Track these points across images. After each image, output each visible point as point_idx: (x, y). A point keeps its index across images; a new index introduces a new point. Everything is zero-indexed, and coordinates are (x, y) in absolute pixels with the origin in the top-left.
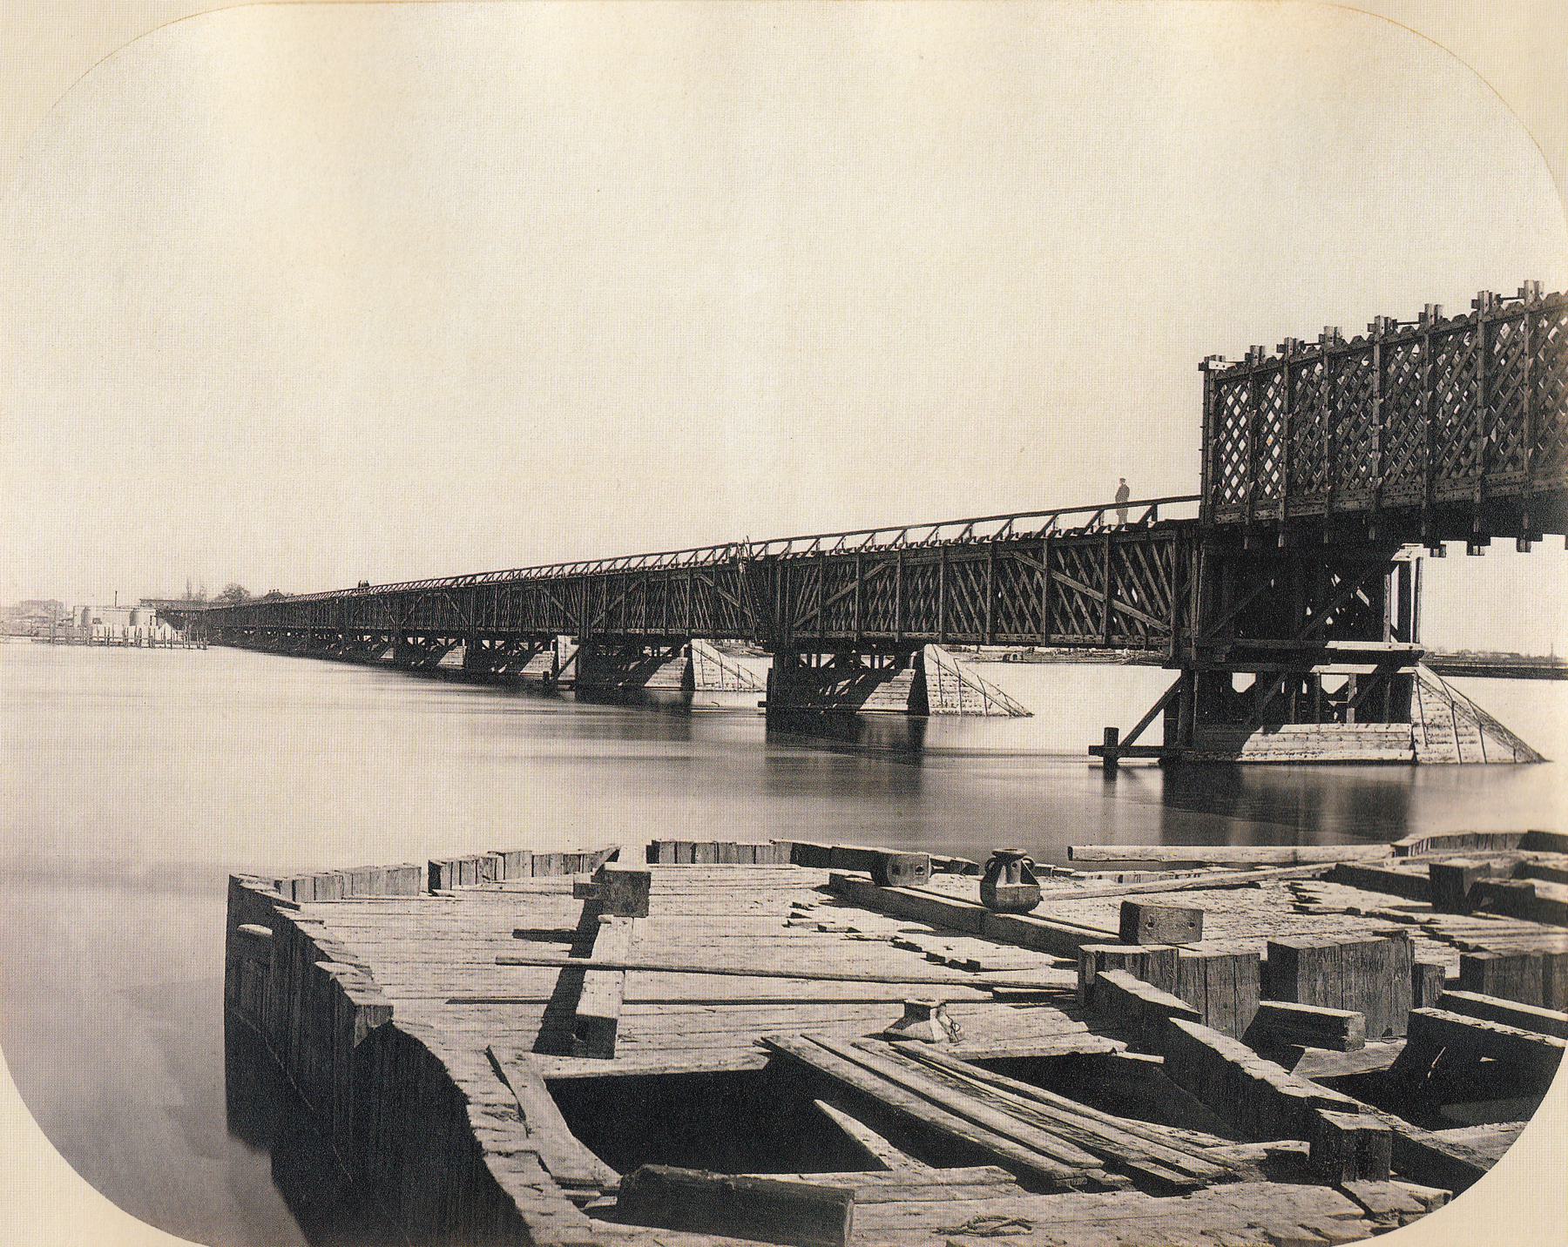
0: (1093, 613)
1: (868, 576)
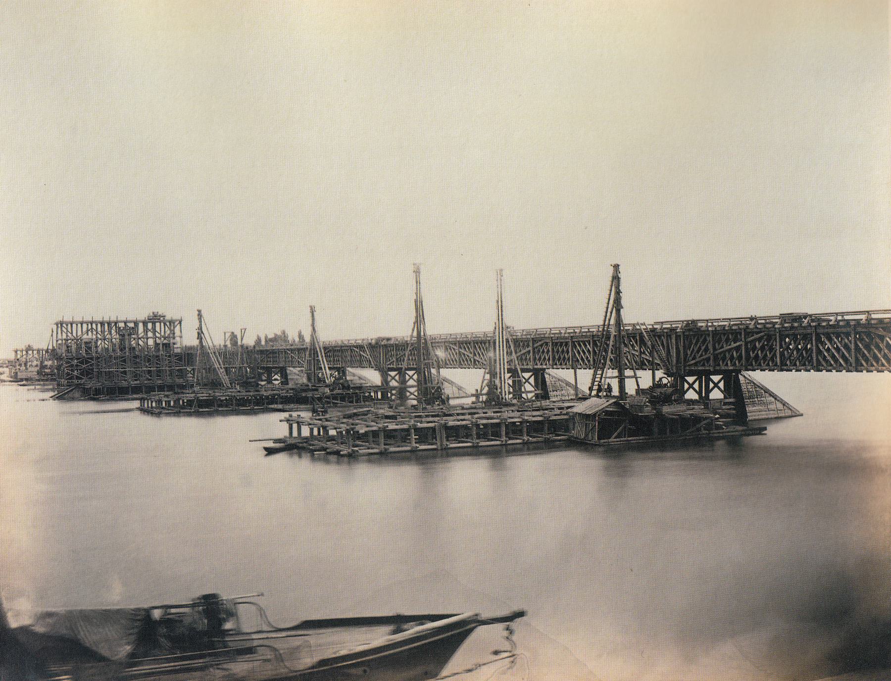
0: (470, 360)
1: (535, 346)
